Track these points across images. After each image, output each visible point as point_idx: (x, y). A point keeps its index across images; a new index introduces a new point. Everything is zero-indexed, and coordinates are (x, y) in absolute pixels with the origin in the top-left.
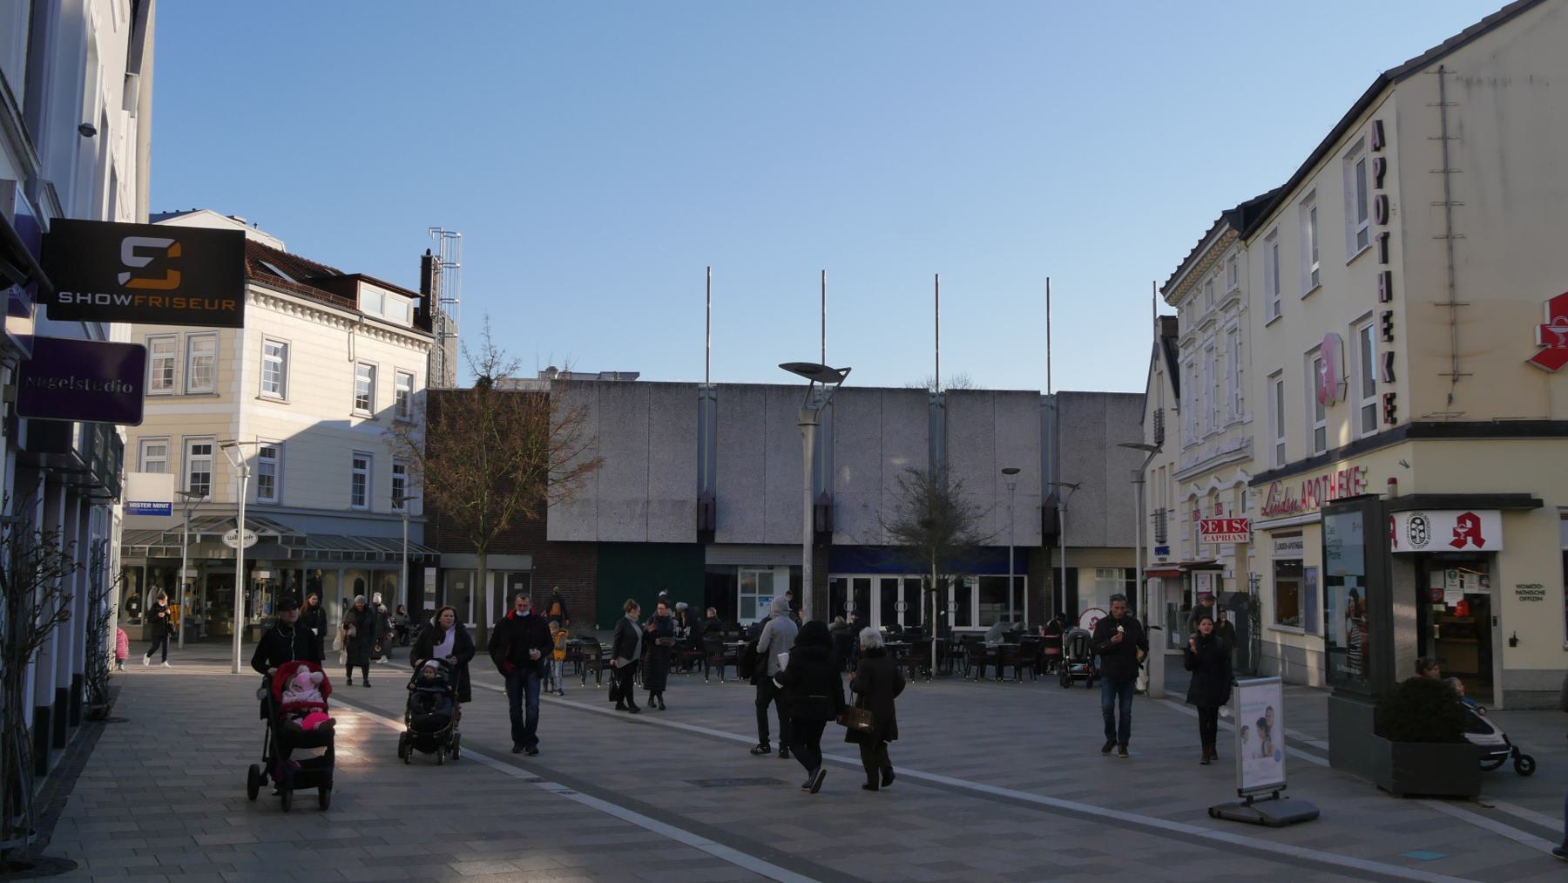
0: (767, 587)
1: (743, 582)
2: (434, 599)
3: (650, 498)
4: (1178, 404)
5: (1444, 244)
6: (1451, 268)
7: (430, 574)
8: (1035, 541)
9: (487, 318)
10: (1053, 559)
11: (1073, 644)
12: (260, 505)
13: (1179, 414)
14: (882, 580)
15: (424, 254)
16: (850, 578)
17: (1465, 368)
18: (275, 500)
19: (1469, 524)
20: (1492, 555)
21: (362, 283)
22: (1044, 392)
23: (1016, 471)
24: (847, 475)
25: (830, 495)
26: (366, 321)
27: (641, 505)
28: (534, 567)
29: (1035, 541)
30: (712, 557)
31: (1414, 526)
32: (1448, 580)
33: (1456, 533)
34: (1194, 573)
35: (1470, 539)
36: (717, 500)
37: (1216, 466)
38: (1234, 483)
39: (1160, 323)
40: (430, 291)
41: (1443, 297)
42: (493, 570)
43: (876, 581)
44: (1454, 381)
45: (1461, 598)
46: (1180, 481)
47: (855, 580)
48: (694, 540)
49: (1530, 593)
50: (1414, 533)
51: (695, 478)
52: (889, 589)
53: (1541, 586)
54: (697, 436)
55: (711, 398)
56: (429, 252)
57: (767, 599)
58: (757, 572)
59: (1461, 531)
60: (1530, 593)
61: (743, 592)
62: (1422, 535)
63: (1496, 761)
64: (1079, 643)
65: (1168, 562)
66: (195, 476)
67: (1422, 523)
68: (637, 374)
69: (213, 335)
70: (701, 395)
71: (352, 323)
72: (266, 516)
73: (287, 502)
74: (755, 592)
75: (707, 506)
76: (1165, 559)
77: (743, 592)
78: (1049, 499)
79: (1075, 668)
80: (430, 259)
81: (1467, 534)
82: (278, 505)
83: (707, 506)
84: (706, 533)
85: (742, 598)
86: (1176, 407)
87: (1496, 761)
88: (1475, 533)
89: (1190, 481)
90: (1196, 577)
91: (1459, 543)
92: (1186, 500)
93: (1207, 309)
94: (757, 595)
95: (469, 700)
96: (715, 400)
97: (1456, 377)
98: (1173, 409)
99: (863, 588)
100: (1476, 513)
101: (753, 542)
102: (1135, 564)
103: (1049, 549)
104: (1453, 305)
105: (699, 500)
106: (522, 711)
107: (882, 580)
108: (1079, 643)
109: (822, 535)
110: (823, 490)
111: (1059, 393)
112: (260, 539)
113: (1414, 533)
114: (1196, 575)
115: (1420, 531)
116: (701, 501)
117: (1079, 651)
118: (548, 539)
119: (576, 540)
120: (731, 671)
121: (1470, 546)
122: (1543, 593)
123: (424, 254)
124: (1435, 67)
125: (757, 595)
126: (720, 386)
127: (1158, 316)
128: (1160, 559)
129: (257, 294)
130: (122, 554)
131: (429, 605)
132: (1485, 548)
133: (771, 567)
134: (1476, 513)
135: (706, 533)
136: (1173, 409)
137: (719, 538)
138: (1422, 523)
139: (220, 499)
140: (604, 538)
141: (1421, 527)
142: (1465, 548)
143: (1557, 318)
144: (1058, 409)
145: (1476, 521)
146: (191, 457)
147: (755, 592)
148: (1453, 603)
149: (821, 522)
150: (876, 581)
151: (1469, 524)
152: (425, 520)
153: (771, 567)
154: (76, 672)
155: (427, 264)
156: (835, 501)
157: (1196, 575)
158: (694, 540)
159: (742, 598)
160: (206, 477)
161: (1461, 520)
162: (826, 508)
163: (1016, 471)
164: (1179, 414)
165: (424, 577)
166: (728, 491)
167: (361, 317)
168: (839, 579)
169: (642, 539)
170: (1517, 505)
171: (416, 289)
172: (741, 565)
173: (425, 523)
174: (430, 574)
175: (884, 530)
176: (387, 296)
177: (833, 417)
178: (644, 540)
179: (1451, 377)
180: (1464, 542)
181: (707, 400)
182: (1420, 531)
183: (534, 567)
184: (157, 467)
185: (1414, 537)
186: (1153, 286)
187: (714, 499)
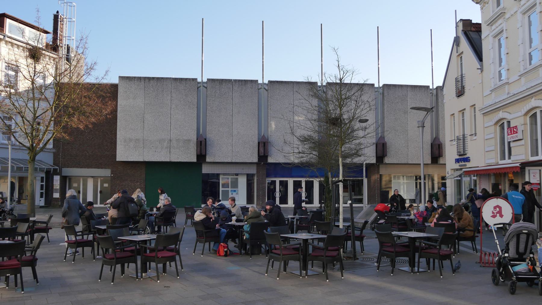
0: (235, 184)
1: (223, 183)
2: (59, 192)
3: (171, 138)
4: (482, 66)
7: (57, 180)
8: (373, 161)
9: (38, 11)
10: (380, 170)
11: (515, 239)
13: (482, 72)
14: (294, 181)
15: (55, 13)
16: (278, 180)
19: (498, 209)
21: (7, 19)
24: (273, 125)
25: (266, 137)
26: (7, 39)
27: (166, 142)
28: (112, 175)
29: (373, 161)
30: (206, 169)
33: (493, 213)
34: (527, 169)
36: (207, 140)
37: (510, 103)
38: (494, 123)
39: (461, 25)
40: (57, 32)
42: (92, 177)
43: (291, 182)
46: (483, 114)
47: (280, 181)
48: (195, 160)
51: (196, 128)
52: (297, 185)
54: (196, 106)
55: (204, 86)
56: (58, 12)
57: (235, 191)
58: (230, 177)
64: (523, 238)
65: (467, 167)
70: (199, 85)
74: (228, 187)
75: (201, 142)
76: (465, 165)
78: (379, 139)
79: (518, 269)
80: (58, 16)
83: (201, 142)
84: (201, 157)
85: (222, 190)
86: (479, 67)
89: (500, 110)
90: (529, 173)
92: (493, 124)
93: (493, 12)
94: (230, 189)
95: (456, 159)
96: (206, 88)
98: (478, 69)
99: (284, 185)
101: (226, 161)
102: (421, 174)
103: (379, 165)
105: (197, 139)
106: (350, 178)
107: (294, 181)
108: (523, 238)
109: (263, 157)
110: (263, 135)
111: (384, 85)
114: (529, 170)
116: (198, 140)
117: (522, 249)
118: (117, 160)
119: (132, 160)
123: (55, 13)
125: (230, 189)
127: (458, 20)
128: (460, 166)
131: (56, 195)
133: (237, 175)
135: (201, 157)
136: (478, 69)
137: (208, 160)
140: (147, 160)
144: (383, 94)
147: (229, 188)
149: (262, 150)
150: (291, 182)
151: (498, 209)
152: (54, 151)
153: (237, 175)
155: (56, 18)
156: (269, 140)
157: (529, 170)
158: (195, 160)
159: (222, 190)
162: (264, 143)
164: (482, 72)
165: (53, 180)
166: (212, 135)
167: (4, 36)
168: (272, 181)
169: (167, 160)
171: (50, 29)
172: (222, 174)
173: (54, 153)
174: (57, 180)
175: (295, 139)
176: (26, 28)
177: (268, 96)
178: (169, 161)
181: (202, 87)
183: (112, 175)
186: (430, 31)
187: (205, 139)
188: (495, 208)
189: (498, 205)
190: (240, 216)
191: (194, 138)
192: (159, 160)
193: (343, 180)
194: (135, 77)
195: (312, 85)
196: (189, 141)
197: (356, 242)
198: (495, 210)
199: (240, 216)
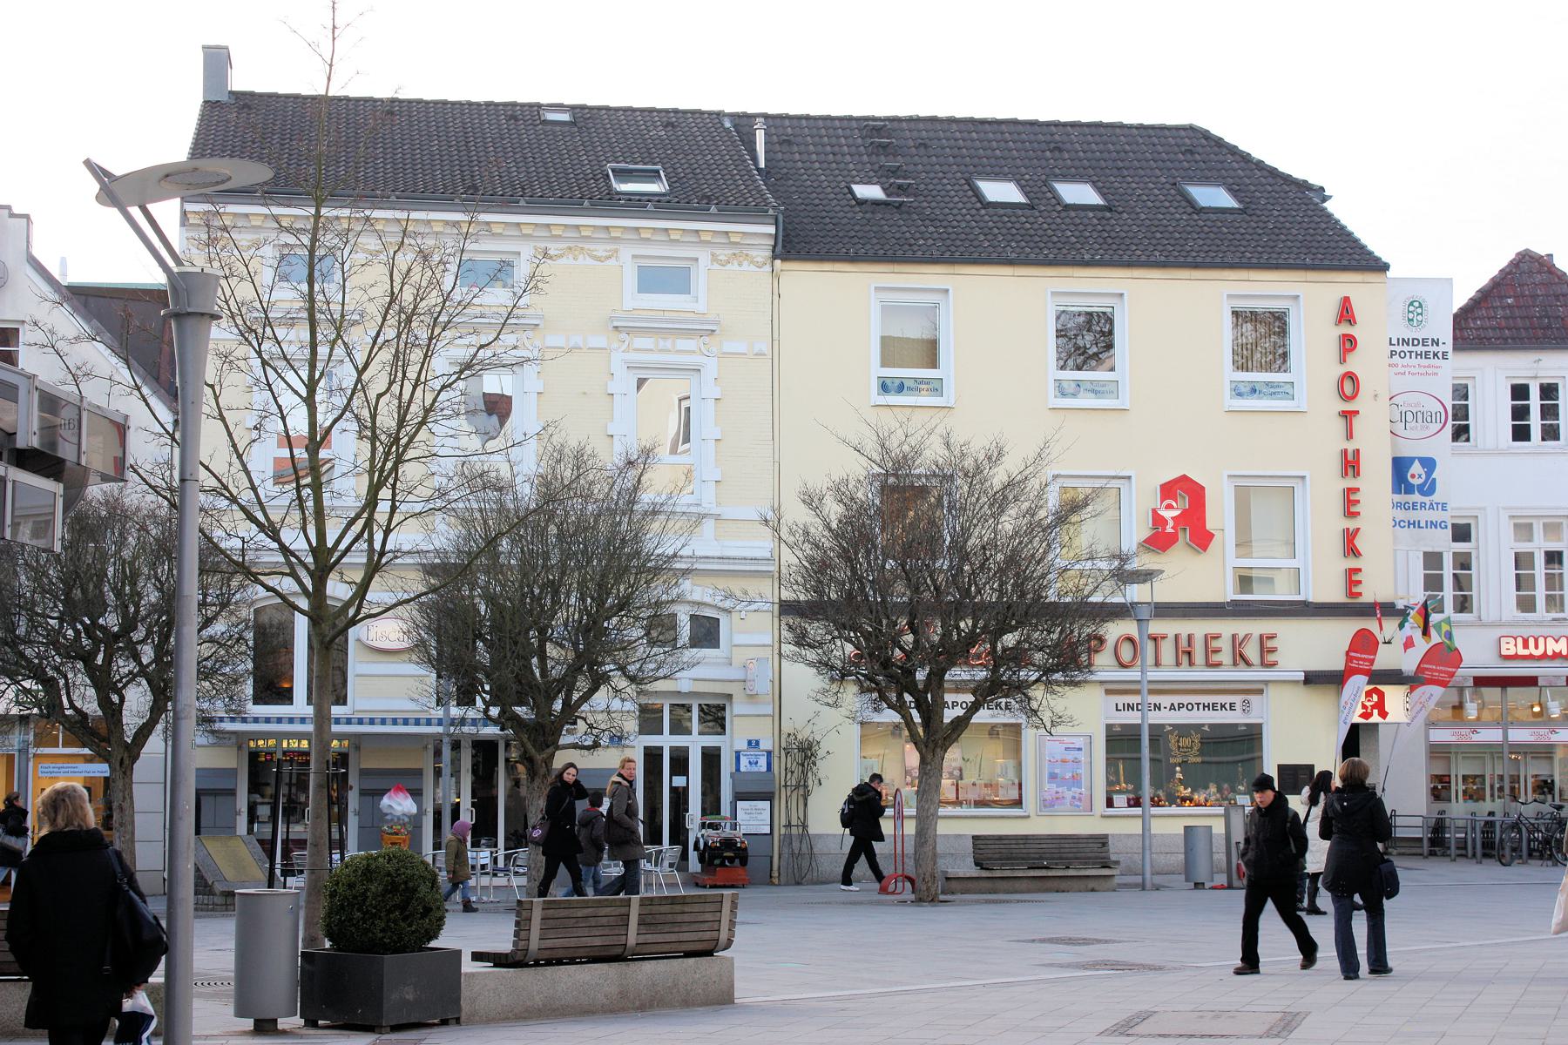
19: (1375, 698)
31: (1411, 308)
35: (1376, 712)
50: (1411, 316)
59: (1368, 704)
62: (1420, 318)
63: (365, 515)
69: (724, 353)
81: (1373, 707)
87: (365, 515)
88: (1380, 706)
91: (1366, 715)
100: (1381, 687)
113: (1411, 316)
115: (1418, 314)
120: (590, 792)
130: (687, 759)
134: (1381, 687)
138: (1421, 306)
141: (1419, 310)
142: (1371, 720)
143: (1165, 503)
145: (1381, 695)
154: (233, 798)
180: (1371, 715)
182: (1418, 314)
184: (911, 807)
185: (1410, 320)
188: (1168, 490)
198: (1169, 507)
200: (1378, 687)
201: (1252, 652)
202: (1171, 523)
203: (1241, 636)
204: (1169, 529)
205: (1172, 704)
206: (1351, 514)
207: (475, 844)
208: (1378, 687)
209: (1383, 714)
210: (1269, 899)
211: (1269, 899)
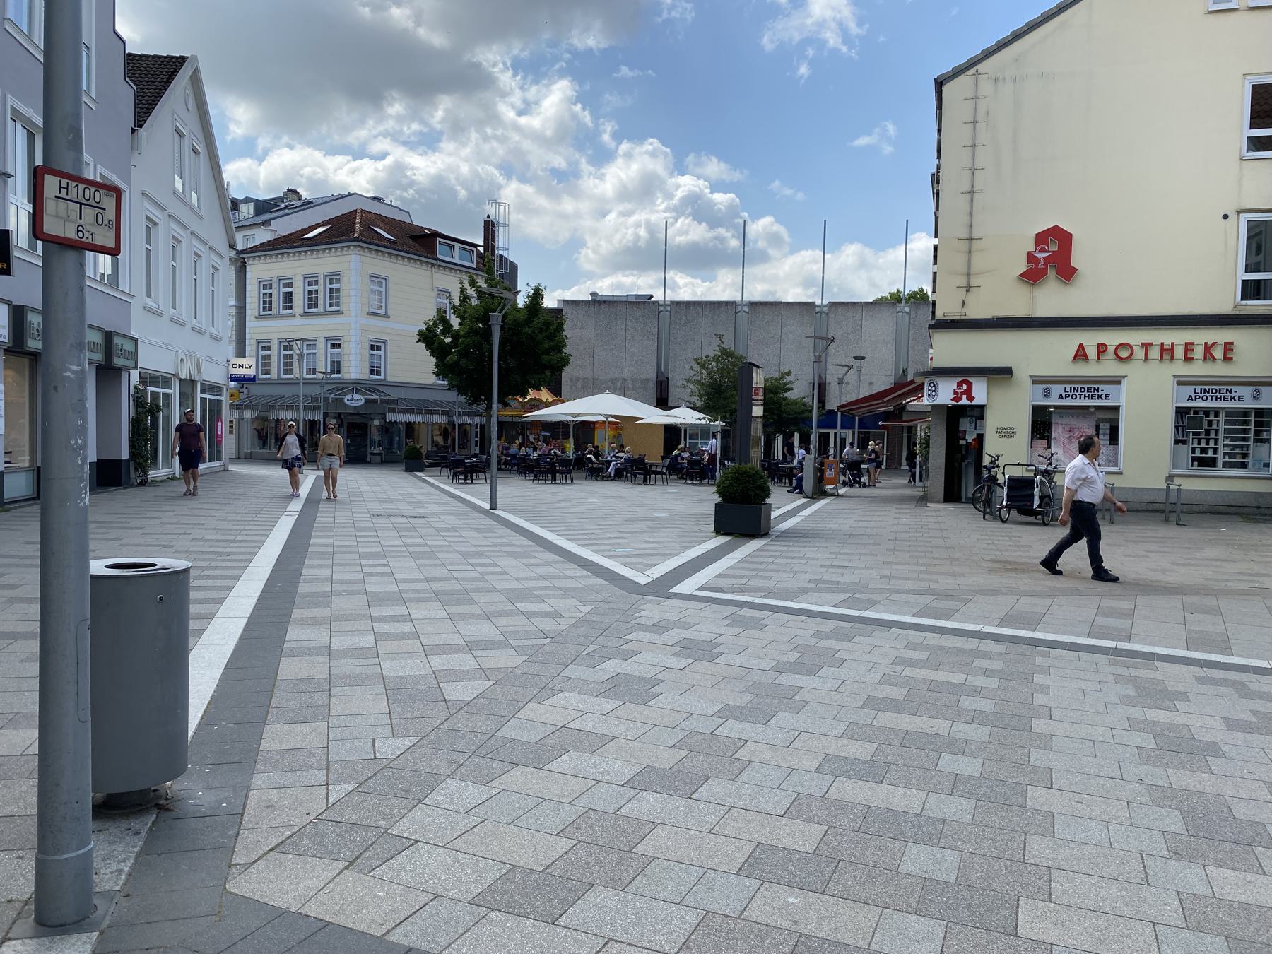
5: (968, 197)
6: (971, 214)
12: (372, 380)
15: (486, 218)
17: (974, 282)
18: (382, 377)
19: (965, 387)
20: (982, 408)
22: (818, 302)
23: (863, 358)
32: (969, 425)
33: (955, 393)
35: (964, 397)
41: (966, 236)
44: (967, 291)
45: (975, 436)
49: (1007, 433)
53: (1013, 428)
60: (1007, 433)
61: (202, 392)
66: (333, 363)
67: (934, 386)
68: (652, 297)
71: (433, 265)
72: (377, 387)
73: (390, 378)
75: (661, 382)
77: (202, 392)
82: (384, 380)
91: (956, 399)
94: (699, 441)
97: (968, 289)
100: (970, 379)
104: (970, 239)
112: (367, 401)
121: (964, 401)
122: (1015, 433)
123: (486, 218)
124: (973, 71)
125: (699, 441)
126: (673, 303)
129: (249, 258)
132: (974, 403)
134: (970, 379)
139: (346, 376)
141: (933, 389)
143: (1039, 248)
145: (970, 385)
146: (330, 350)
148: (970, 440)
151: (965, 387)
160: (339, 363)
161: (960, 384)
163: (863, 358)
170: (1000, 374)
179: (965, 289)
180: (961, 399)
187: (667, 378)
188: (1042, 238)
189: (1056, 227)
190: (1055, 472)
191: (652, 374)
192: (943, 479)
193: (831, 412)
194: (582, 301)
195: (810, 306)
196: (647, 380)
197: (8, 495)
198: (1043, 250)
199: (1055, 472)
200: (968, 379)
201: (1218, 353)
202: (1043, 261)
203: (1210, 343)
204: (1041, 266)
205: (1190, 396)
206: (149, 243)
207: (713, 457)
208: (968, 379)
209: (971, 398)
210: (1085, 539)
211: (1085, 539)
